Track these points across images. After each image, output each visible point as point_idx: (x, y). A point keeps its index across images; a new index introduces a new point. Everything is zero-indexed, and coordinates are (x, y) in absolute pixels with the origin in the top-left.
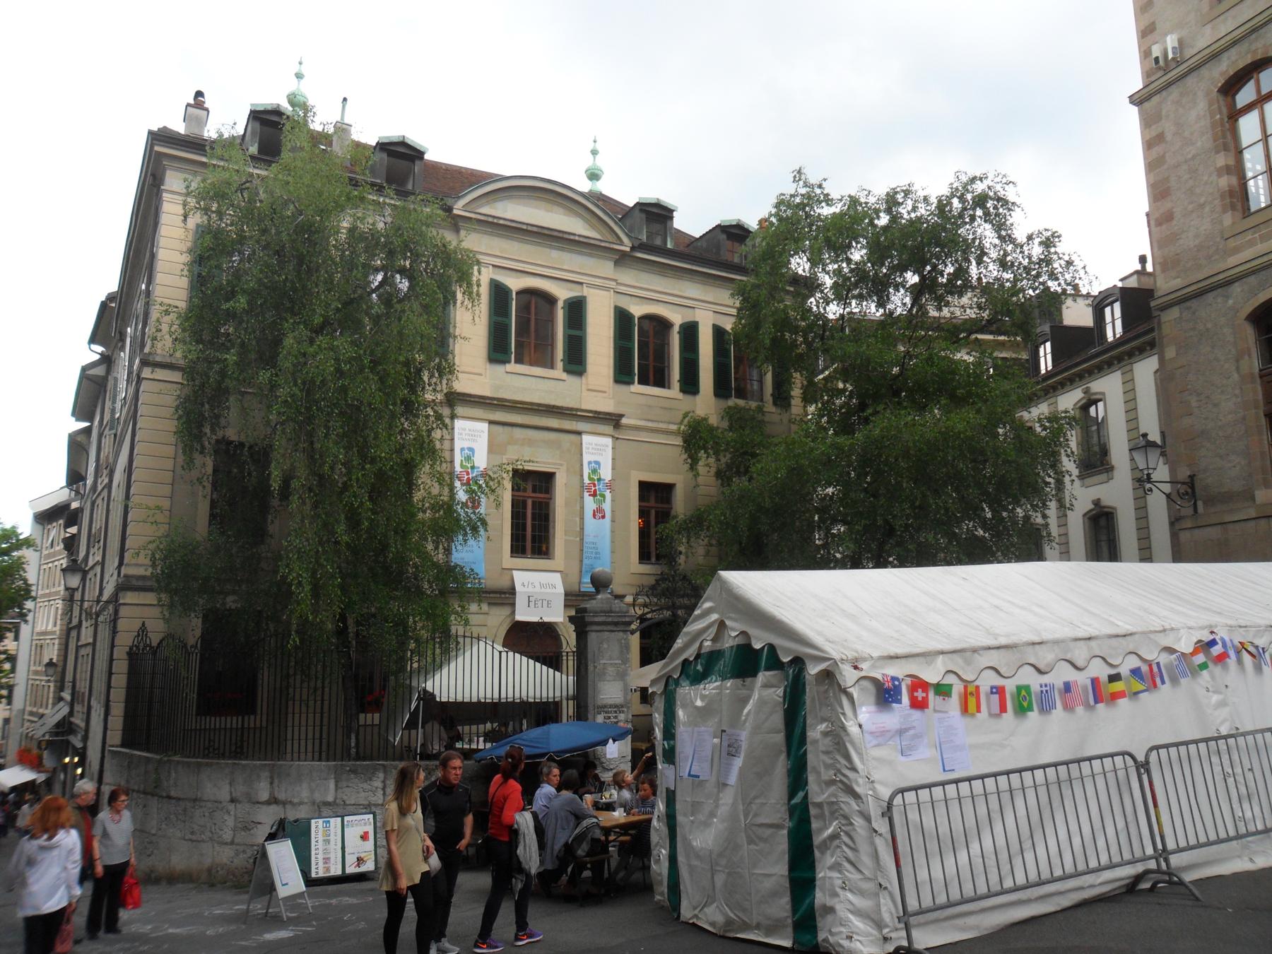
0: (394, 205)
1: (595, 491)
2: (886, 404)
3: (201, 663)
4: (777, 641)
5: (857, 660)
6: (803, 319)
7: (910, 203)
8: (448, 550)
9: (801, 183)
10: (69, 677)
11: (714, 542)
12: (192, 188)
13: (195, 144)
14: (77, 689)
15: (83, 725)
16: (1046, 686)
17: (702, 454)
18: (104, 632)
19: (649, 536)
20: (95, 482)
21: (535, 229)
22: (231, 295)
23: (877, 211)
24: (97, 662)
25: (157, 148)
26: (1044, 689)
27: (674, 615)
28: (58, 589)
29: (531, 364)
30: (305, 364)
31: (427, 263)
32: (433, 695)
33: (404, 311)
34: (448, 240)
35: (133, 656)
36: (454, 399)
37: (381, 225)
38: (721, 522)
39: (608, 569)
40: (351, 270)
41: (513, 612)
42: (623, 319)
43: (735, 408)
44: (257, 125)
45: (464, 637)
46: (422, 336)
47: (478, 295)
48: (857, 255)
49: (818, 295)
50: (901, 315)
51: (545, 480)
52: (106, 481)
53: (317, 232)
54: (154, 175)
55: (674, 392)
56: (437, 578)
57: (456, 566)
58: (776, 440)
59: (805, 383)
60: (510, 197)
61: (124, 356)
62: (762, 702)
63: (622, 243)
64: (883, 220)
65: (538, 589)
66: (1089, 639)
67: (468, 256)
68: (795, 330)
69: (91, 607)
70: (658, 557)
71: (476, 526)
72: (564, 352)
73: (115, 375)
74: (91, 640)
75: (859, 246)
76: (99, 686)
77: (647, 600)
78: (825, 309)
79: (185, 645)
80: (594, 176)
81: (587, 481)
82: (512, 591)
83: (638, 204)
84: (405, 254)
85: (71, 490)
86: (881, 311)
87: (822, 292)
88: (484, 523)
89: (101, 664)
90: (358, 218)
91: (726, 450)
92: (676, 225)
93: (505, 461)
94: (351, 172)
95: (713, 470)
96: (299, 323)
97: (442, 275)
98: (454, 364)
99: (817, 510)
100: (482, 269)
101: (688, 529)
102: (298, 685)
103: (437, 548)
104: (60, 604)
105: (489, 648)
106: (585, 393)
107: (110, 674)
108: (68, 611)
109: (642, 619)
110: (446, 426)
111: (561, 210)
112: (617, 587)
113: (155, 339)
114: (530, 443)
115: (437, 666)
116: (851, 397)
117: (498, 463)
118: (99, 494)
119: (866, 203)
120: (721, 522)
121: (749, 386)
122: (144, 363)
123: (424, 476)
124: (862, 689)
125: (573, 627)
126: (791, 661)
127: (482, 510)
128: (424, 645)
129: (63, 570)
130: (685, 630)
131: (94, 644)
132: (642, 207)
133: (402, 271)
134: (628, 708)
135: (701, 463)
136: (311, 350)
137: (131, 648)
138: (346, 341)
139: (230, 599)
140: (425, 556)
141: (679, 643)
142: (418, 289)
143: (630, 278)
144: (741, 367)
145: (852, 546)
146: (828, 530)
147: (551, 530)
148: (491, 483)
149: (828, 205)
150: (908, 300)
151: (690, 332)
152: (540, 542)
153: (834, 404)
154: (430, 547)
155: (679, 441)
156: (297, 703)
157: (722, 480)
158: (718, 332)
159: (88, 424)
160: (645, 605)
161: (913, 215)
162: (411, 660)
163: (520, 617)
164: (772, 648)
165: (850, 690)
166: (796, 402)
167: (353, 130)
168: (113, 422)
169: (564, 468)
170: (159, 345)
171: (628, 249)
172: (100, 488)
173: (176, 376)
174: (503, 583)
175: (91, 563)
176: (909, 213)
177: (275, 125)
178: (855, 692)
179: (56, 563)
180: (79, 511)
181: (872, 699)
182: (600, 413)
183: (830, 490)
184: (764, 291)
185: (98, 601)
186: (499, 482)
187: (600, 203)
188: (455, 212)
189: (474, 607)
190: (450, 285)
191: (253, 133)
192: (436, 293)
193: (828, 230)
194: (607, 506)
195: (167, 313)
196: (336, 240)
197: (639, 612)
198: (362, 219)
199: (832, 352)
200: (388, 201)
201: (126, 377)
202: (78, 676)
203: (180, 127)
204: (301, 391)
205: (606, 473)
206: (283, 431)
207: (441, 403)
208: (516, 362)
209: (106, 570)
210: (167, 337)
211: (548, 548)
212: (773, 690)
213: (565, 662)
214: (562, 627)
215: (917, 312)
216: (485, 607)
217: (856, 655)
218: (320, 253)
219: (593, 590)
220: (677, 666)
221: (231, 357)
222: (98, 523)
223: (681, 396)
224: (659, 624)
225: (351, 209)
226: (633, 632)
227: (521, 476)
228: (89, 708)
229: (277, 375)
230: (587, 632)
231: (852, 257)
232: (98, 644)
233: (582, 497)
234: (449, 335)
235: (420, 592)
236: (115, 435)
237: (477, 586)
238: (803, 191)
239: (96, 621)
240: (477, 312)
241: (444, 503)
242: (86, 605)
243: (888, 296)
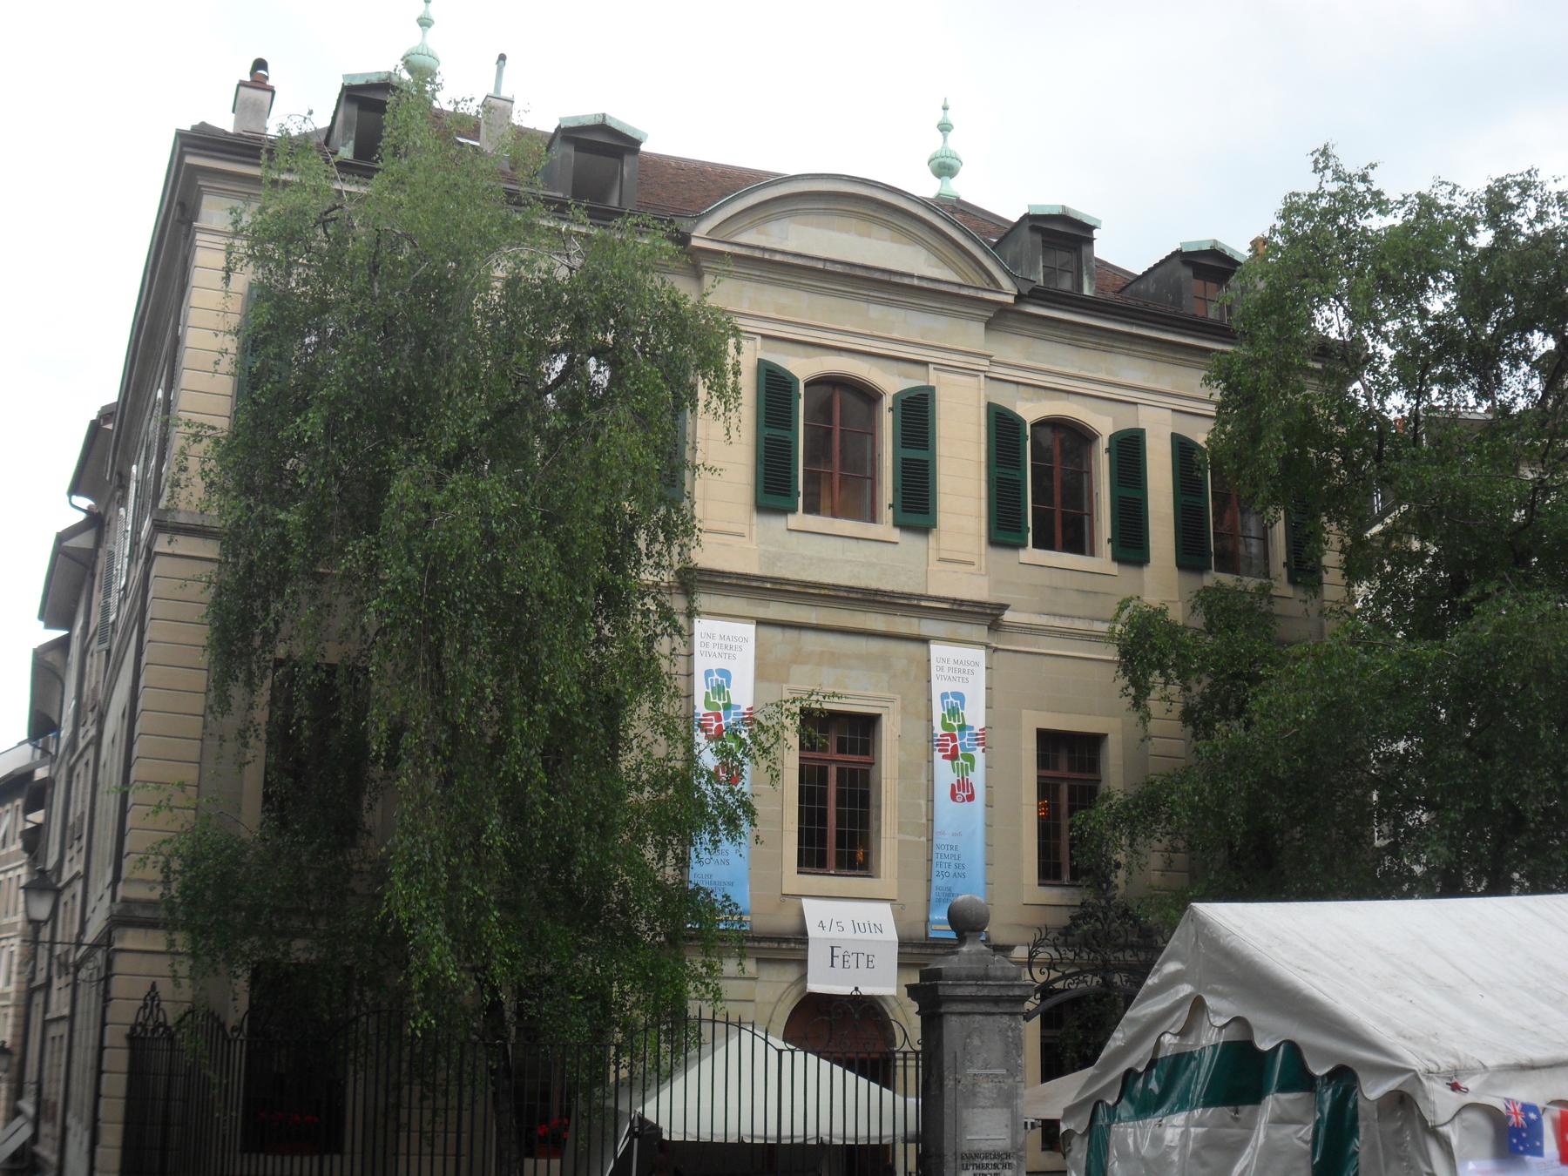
0: (587, 236)
1: (955, 749)
2: (1503, 579)
3: (247, 1057)
4: (1304, 1037)
5: (1456, 1071)
6: (1340, 422)
7: (1532, 205)
8: (683, 859)
9: (1329, 173)
10: (31, 1074)
11: (1181, 844)
12: (243, 224)
13: (245, 147)
14: (44, 1096)
15: (53, 1158)
17: (1156, 677)
18: (88, 999)
19: (1057, 835)
20: (75, 733)
21: (839, 268)
22: (302, 406)
23: (1471, 222)
24: (76, 1051)
25: (189, 160)
27: (1107, 983)
28: (14, 919)
29: (834, 515)
30: (428, 523)
31: (645, 335)
32: (656, 1129)
33: (602, 424)
34: (682, 292)
35: (136, 1040)
36: (693, 580)
37: (562, 273)
38: (1193, 808)
39: (980, 898)
40: (509, 354)
41: (803, 977)
42: (1003, 426)
43: (1216, 589)
44: (354, 111)
45: (714, 1021)
46: (635, 470)
47: (736, 390)
48: (1437, 303)
49: (1368, 377)
50: (1526, 411)
52: (92, 732)
53: (451, 289)
54: (182, 205)
55: (1102, 560)
56: (663, 912)
57: (699, 889)
58: (1295, 650)
59: (1348, 541)
61: (126, 514)
62: (1270, 1152)
63: (999, 289)
64: (1484, 238)
65: (849, 934)
67: (717, 321)
68: (1328, 442)
69: (67, 953)
70: (1075, 874)
71: (737, 815)
72: (895, 490)
73: (109, 546)
74: (66, 1011)
75: (1440, 285)
76: (81, 1090)
77: (1055, 955)
78: (1381, 402)
79: (222, 1026)
80: (944, 168)
81: (939, 730)
82: (801, 937)
83: (1027, 217)
84: (606, 323)
85: (36, 747)
86: (1486, 404)
87: (1375, 370)
88: (750, 811)
89: (84, 1055)
90: (523, 262)
91: (1201, 669)
92: (1097, 254)
93: (787, 696)
94: (512, 181)
95: (1178, 708)
96: (418, 451)
97: (670, 357)
98: (693, 517)
99: (1376, 782)
100: (744, 342)
101: (1131, 821)
102: (415, 1102)
103: (662, 857)
104: (16, 945)
105: (760, 1044)
106: (935, 566)
107: (99, 1072)
108: (30, 958)
109: (1046, 991)
110: (679, 631)
111: (886, 233)
112: (997, 931)
113: (175, 484)
114: (834, 660)
115: (664, 1076)
116: (1435, 566)
117: (775, 700)
118: (81, 756)
119: (1449, 207)
120: (1193, 808)
121: (1242, 549)
122: (159, 527)
123: (639, 721)
124: (1466, 1128)
125: (915, 1007)
126: (1328, 1074)
127: (745, 786)
128: (641, 1037)
129: (26, 888)
130: (1129, 1014)
131: (71, 1018)
132: (1037, 223)
133: (600, 352)
134: (1020, 1158)
135: (1153, 694)
136: (439, 498)
137: (133, 1029)
138: (500, 482)
139: (299, 944)
140: (641, 871)
141: (1118, 1038)
142: (628, 383)
143: (1013, 350)
144: (1228, 516)
145: (1443, 850)
146: (1399, 820)
147: (873, 823)
148: (763, 737)
149: (1380, 212)
150: (1536, 384)
151: (1129, 447)
152: (853, 845)
153: (1403, 580)
154: (650, 854)
155: (1112, 653)
156: (415, 1136)
157: (1195, 726)
158: (1182, 448)
159: (66, 632)
160: (1051, 965)
161: (1539, 228)
162: (617, 1063)
163: (814, 986)
164: (1293, 1048)
165: (1444, 1130)
166: (1333, 580)
167: (516, 107)
168: (106, 630)
169: (898, 704)
170: (184, 494)
171: (1011, 300)
172: (82, 744)
173: (210, 549)
174: (783, 922)
175: (66, 876)
176: (1531, 223)
177: (380, 107)
178: (1453, 1134)
179: (10, 874)
180: (48, 783)
181: (1486, 1147)
182: (962, 602)
183: (1401, 746)
184: (1267, 372)
185: (79, 944)
186: (776, 734)
187: (957, 217)
188: (695, 242)
189: (730, 966)
190: (686, 374)
191: (347, 122)
192: (661, 390)
193: (1383, 257)
194: (978, 778)
195: (197, 438)
196: (484, 302)
197: (1041, 979)
198: (529, 264)
199: (1398, 483)
200: (575, 228)
201: (127, 551)
202: (46, 1073)
203: (226, 122)
204: (422, 572)
205: (975, 716)
206: (387, 648)
207: (670, 588)
208: (806, 511)
209: (91, 890)
210: (197, 480)
211: (867, 855)
212: (1294, 1127)
213: (900, 1071)
214: (894, 1004)
215: (1556, 404)
216: (750, 966)
217: (1453, 1061)
218: (455, 325)
219: (953, 935)
220: (1113, 1082)
221: (292, 517)
222: (79, 807)
223: (1114, 568)
224: (1077, 1001)
225: (511, 245)
226: (1028, 1017)
228: (64, 1130)
229: (378, 546)
230: (941, 1016)
231: (1429, 307)
232: (78, 1019)
233: (931, 762)
234: (684, 464)
235: (632, 938)
236: (108, 652)
237: (736, 926)
238: (1333, 187)
239: (75, 978)
240: (734, 421)
241: (676, 773)
242: (58, 949)
243: (1498, 377)
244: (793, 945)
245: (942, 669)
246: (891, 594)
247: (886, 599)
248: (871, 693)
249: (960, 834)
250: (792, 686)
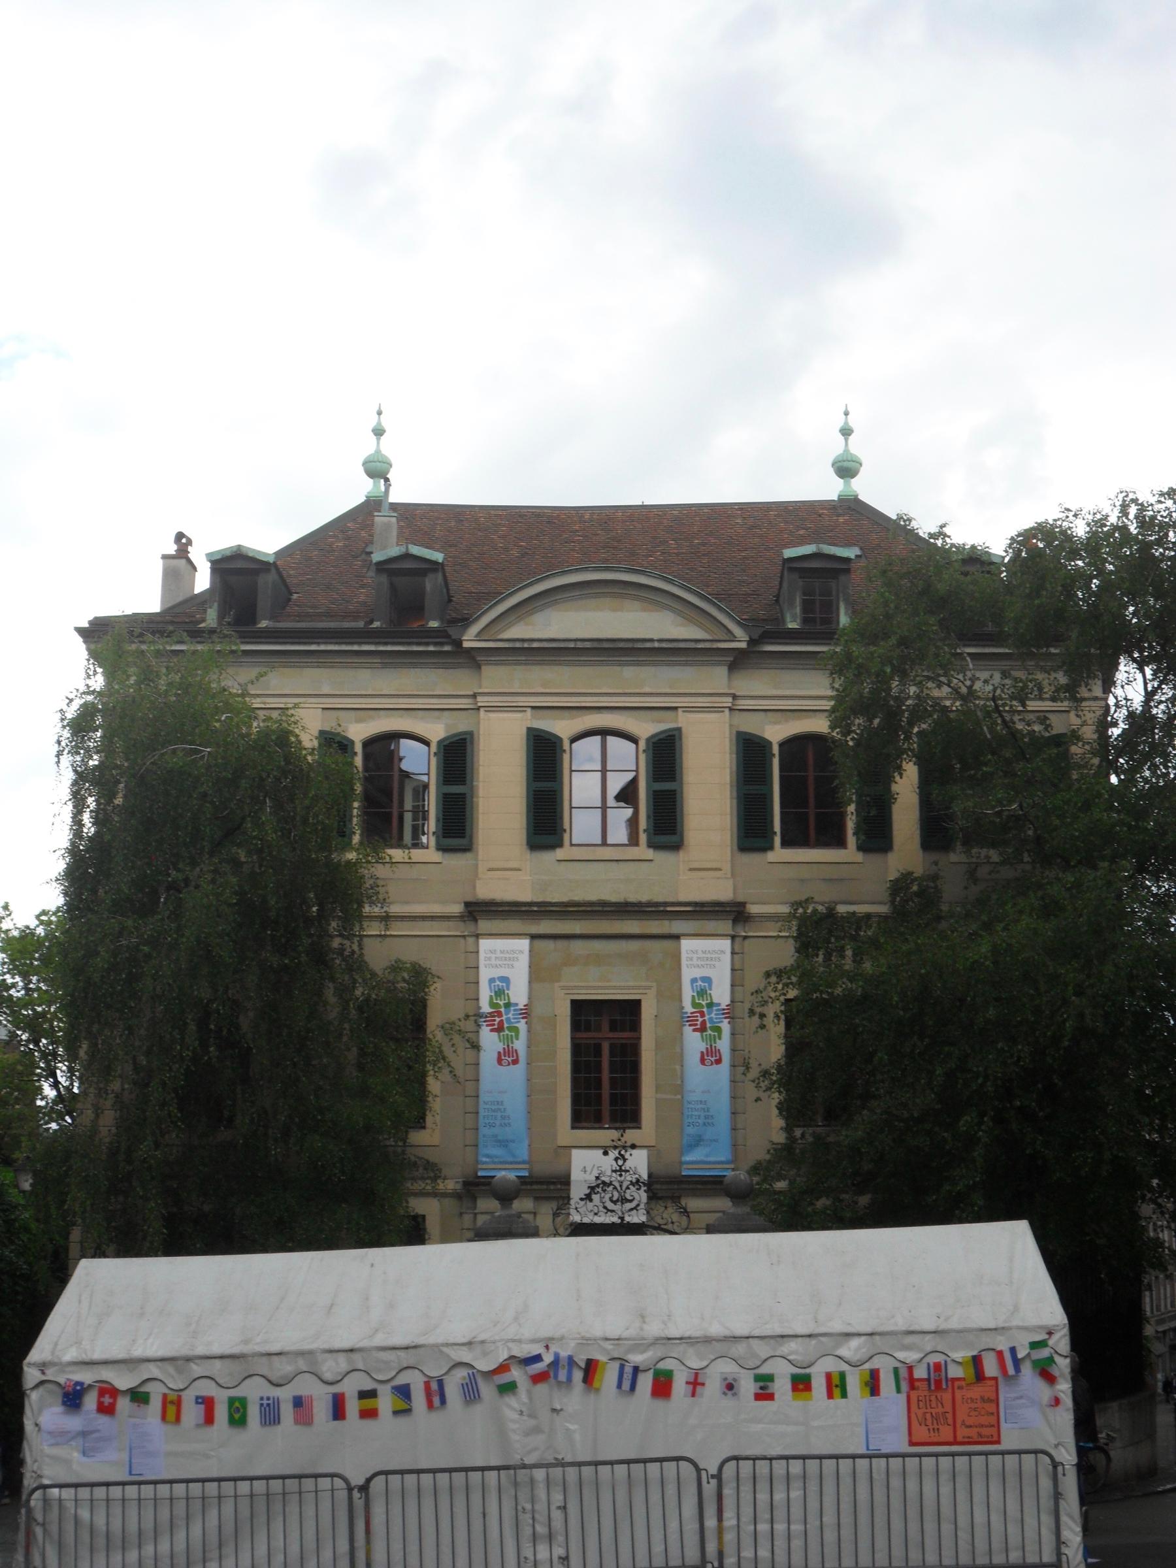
1: (704, 1023)
16: (268, 1399)
21: (588, 645)
26: (265, 1402)
51: (627, 1013)
60: (556, 602)
63: (734, 639)
66: (351, 1350)
80: (846, 469)
81: (689, 1009)
82: (564, 1181)
111: (637, 604)
169: (652, 993)
171: (743, 645)
182: (702, 904)
188: (466, 645)
223: (859, 857)
227: (585, 1013)
244: (559, 1186)
245: (691, 959)
246: (640, 904)
247: (636, 909)
248: (631, 984)
249: (709, 1092)
250: (562, 984)
